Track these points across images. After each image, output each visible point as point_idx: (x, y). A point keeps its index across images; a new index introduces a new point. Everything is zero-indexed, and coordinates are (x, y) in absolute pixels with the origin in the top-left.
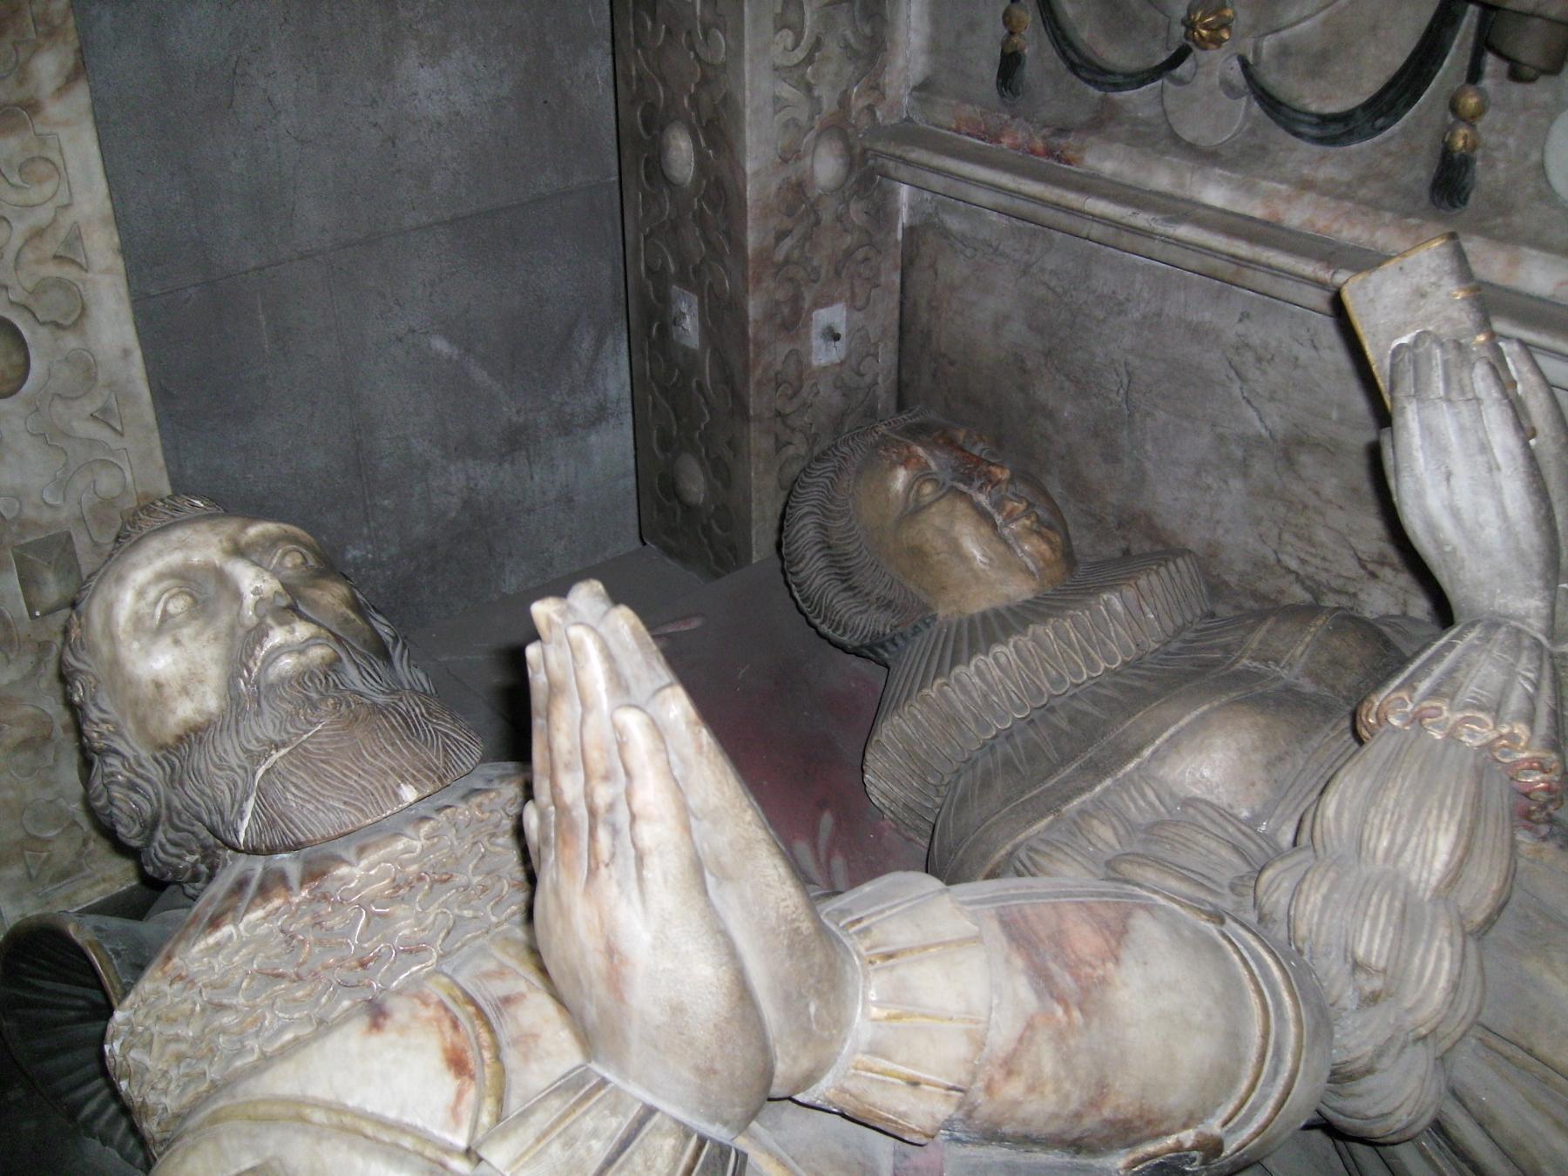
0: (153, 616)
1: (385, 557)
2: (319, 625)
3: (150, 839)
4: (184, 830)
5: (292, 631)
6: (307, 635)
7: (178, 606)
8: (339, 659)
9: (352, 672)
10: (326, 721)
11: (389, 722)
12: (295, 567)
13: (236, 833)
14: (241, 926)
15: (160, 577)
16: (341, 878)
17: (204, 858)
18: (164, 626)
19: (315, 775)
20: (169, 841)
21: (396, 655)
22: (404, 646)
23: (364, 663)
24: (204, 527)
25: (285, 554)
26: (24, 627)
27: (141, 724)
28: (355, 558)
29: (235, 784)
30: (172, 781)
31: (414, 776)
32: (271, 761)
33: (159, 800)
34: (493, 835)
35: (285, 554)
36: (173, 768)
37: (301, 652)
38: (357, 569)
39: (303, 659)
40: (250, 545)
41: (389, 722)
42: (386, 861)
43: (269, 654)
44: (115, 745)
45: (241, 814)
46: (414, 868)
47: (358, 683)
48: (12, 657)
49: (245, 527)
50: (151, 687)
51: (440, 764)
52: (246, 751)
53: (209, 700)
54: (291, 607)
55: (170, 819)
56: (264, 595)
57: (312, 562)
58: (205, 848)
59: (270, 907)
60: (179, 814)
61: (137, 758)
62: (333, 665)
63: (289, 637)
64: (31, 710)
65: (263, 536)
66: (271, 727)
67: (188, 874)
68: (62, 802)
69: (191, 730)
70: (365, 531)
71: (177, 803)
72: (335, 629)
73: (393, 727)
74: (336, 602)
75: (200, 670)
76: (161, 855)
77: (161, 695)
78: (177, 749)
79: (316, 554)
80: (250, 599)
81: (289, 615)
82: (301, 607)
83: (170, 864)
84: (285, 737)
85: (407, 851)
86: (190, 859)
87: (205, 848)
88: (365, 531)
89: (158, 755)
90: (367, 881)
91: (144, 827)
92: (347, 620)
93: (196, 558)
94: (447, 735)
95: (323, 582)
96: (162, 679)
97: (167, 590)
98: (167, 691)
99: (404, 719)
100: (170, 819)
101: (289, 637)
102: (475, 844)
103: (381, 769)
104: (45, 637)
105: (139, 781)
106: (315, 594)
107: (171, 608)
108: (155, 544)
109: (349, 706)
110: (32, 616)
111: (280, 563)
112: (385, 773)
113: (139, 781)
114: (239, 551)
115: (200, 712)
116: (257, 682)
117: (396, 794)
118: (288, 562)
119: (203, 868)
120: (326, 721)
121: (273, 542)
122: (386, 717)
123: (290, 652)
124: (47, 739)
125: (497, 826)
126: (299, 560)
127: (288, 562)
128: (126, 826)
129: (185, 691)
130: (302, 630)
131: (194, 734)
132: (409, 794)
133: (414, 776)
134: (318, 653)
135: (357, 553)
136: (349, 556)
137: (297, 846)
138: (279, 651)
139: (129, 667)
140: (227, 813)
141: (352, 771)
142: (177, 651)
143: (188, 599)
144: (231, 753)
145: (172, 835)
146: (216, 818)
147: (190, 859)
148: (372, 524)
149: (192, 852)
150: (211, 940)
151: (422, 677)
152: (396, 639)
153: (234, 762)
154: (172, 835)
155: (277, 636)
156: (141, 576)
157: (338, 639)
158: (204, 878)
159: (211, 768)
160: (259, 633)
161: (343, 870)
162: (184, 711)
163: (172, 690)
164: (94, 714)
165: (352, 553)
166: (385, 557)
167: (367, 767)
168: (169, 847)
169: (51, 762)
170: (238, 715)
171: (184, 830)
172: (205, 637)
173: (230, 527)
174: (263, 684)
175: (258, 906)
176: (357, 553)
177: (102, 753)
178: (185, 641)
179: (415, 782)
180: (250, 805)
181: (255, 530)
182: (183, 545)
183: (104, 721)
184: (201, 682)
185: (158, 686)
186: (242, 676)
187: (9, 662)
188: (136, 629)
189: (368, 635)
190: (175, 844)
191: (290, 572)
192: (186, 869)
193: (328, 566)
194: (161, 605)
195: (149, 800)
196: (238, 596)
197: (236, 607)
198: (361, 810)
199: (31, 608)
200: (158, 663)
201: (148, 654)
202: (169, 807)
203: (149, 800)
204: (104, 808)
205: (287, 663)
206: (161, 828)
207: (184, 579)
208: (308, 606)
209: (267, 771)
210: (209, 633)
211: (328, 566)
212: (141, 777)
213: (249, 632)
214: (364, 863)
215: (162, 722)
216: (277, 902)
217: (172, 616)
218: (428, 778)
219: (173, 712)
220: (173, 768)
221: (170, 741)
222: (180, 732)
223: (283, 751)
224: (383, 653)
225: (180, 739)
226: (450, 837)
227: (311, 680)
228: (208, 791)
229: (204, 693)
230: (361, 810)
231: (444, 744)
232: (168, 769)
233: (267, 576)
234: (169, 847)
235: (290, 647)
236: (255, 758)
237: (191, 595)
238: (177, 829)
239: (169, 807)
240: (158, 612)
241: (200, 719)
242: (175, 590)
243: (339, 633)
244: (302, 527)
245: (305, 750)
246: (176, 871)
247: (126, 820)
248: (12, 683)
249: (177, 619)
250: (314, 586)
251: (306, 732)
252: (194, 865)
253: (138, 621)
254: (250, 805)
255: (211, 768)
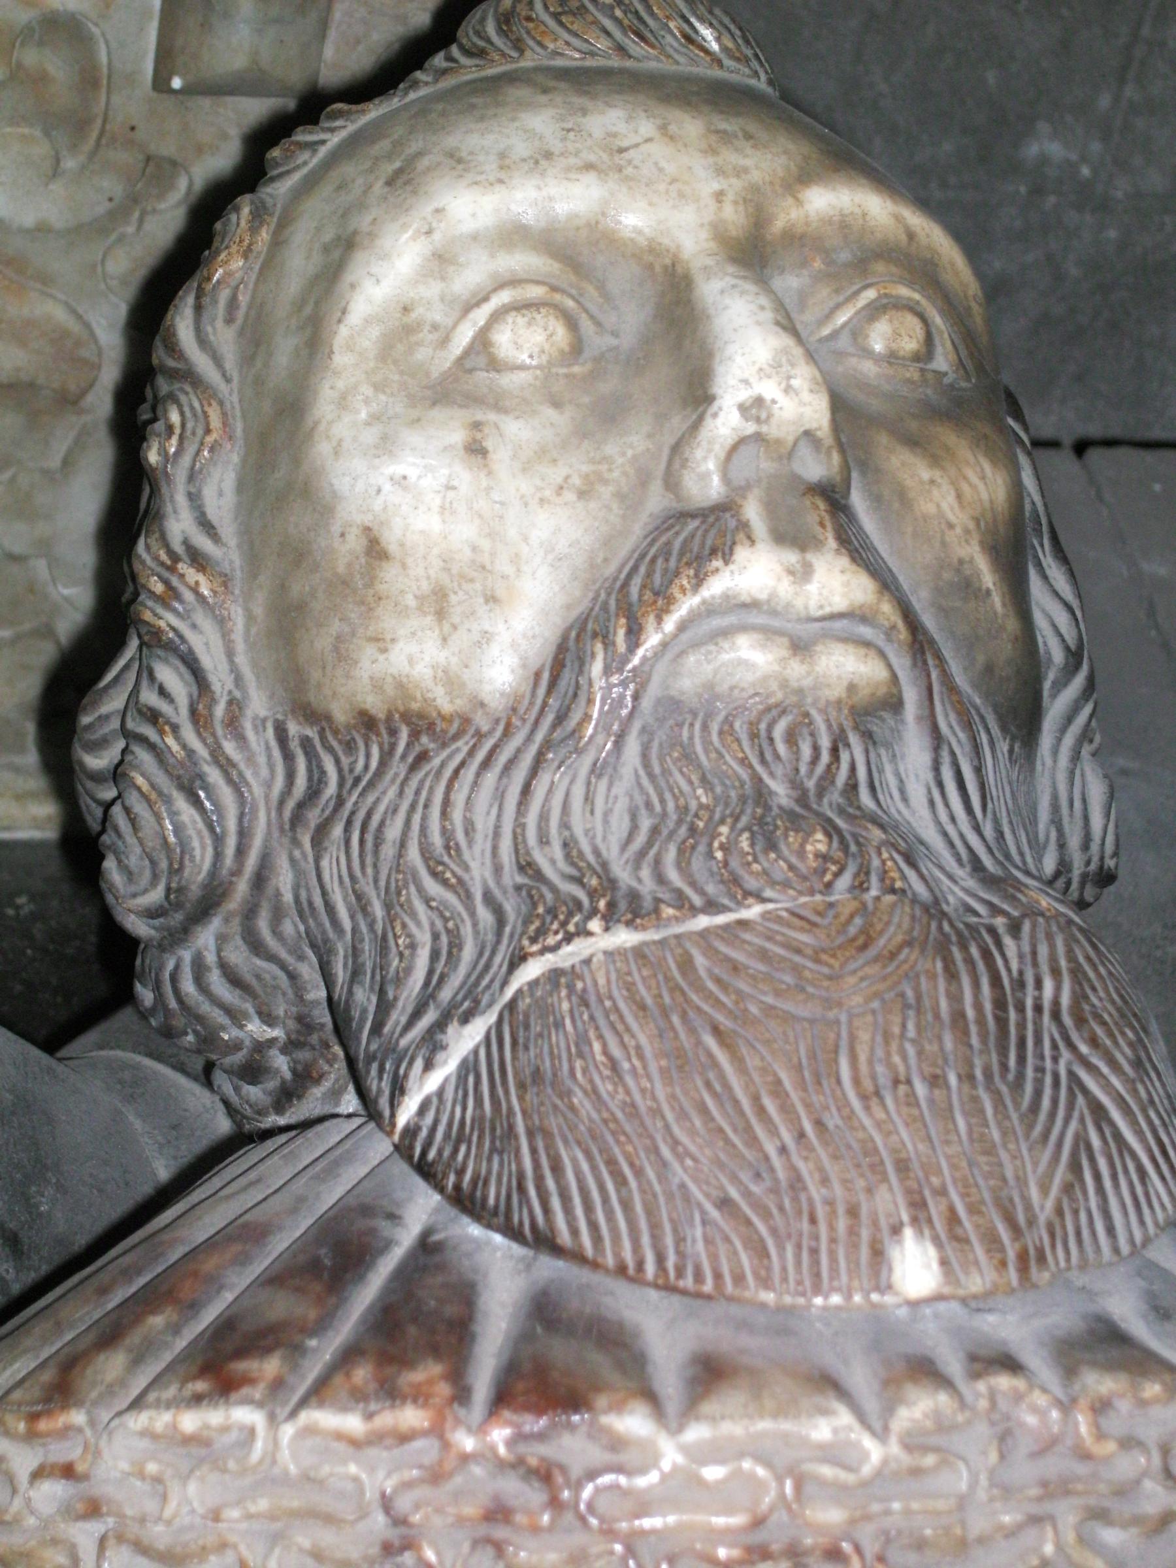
0: (445, 341)
1: (1121, 188)
2: (886, 582)
3: (179, 936)
4: (272, 958)
5: (804, 573)
6: (839, 603)
7: (526, 342)
8: (894, 704)
9: (915, 754)
10: (781, 902)
11: (956, 998)
12: (892, 357)
13: (399, 1089)
14: (288, 1431)
15: (512, 235)
16: (617, 1443)
17: (291, 1046)
18: (461, 389)
19: (680, 1063)
20: (224, 966)
21: (1055, 708)
22: (1090, 687)
23: (956, 737)
24: (691, 126)
25: (875, 311)
26: (131, 103)
27: (287, 623)
28: (1044, 160)
29: (456, 945)
30: (297, 819)
31: (953, 1218)
32: (570, 954)
33: (241, 852)
34: (1100, 1515)
35: (875, 311)
36: (314, 792)
37: (800, 647)
38: (1038, 191)
39: (796, 670)
40: (800, 241)
41: (956, 998)
42: (759, 1459)
43: (709, 610)
44: (195, 641)
45: (432, 1045)
46: (831, 1516)
47: (917, 793)
48: (70, 164)
49: (804, 177)
50: (356, 542)
51: (1045, 1209)
52: (526, 866)
53: (499, 661)
54: (826, 510)
55: (250, 913)
56: (772, 431)
57: (942, 361)
58: (305, 1024)
59: (387, 1419)
60: (278, 915)
61: (236, 706)
62: (871, 715)
63: (785, 589)
64: (60, 314)
65: (843, 224)
66: (620, 825)
67: (238, 1058)
68: (40, 566)
69: (406, 717)
70: (1104, 101)
71: (284, 880)
72: (921, 602)
73: (959, 1016)
74: (959, 518)
75: (503, 566)
76: (188, 986)
77: (371, 579)
78: (350, 747)
79: (966, 336)
80: (725, 422)
81: (815, 513)
82: (858, 500)
83: (200, 1019)
84: (647, 886)
85: (829, 1453)
86: (255, 1028)
87: (305, 1024)
88: (1104, 101)
89: (293, 728)
90: (685, 1487)
91: (175, 897)
92: (968, 587)
93: (634, 219)
94: (1098, 1110)
95: (949, 436)
96: (391, 539)
97: (513, 282)
98: (390, 577)
99: (1000, 1004)
100: (250, 913)
101: (785, 589)
102: (1035, 1520)
103: (870, 1149)
104: (167, 149)
105: (214, 775)
106: (910, 469)
107: (504, 340)
108: (541, 122)
109: (860, 886)
110: (160, 83)
111: (856, 331)
112: (877, 1167)
113: (214, 775)
114: (753, 252)
115: (450, 681)
116: (641, 679)
117: (878, 1254)
118: (879, 338)
119: (281, 1063)
120: (781, 902)
121: (862, 257)
122: (952, 975)
123: (768, 633)
124: (69, 401)
125: (1122, 1491)
126: (910, 345)
127: (879, 338)
128: (130, 875)
129: (438, 604)
130: (834, 584)
131: (413, 732)
132: (916, 1268)
133: (953, 1218)
134: (845, 668)
135: (1055, 150)
136: (1032, 150)
137: (543, 1241)
138: (745, 613)
139: (322, 448)
140: (398, 1016)
141: (786, 1108)
142: (465, 477)
143: (561, 333)
144: (482, 843)
145: (238, 955)
146: (364, 998)
147: (255, 1028)
148: (1130, 91)
149: (268, 1019)
150: (190, 1421)
151: (1097, 791)
152: (1075, 657)
153: (479, 873)
154: (238, 955)
155: (755, 571)
156: (466, 207)
157: (920, 643)
158: (272, 1084)
159: (413, 854)
160: (704, 536)
161: (634, 1423)
162: (409, 658)
163: (403, 582)
164: (179, 524)
165: (1046, 146)
166: (1121, 188)
167: (833, 1120)
168: (215, 979)
169: (55, 462)
170: (547, 745)
171: (272, 958)
172: (556, 474)
173: (765, 159)
174: (653, 691)
175: (358, 1396)
176: (1055, 150)
177: (154, 641)
178: (500, 455)
179: (951, 1239)
180: (466, 1039)
181: (832, 201)
182: (613, 162)
183: (198, 559)
184: (491, 599)
185: (375, 550)
186: (608, 644)
187: (56, 172)
188: (385, 352)
189: (1005, 650)
190: (234, 979)
191: (869, 368)
192: (237, 1046)
193: (989, 396)
194: (481, 315)
195: (219, 841)
196: (697, 393)
197: (678, 423)
198: (761, 1252)
199: (166, 59)
200: (402, 485)
201: (386, 446)
202: (260, 880)
203: (219, 841)
204: (97, 777)
205: (752, 660)
206: (216, 923)
207: (574, 261)
208: (877, 500)
209: (554, 976)
210: (574, 466)
211: (989, 396)
212: (225, 766)
213: (684, 515)
214: (696, 1433)
215: (342, 653)
216: (411, 1416)
217: (495, 365)
218: (992, 1241)
219: (382, 643)
220: (314, 792)
221: (341, 715)
222: (374, 704)
223: (624, 937)
224: (1023, 719)
225: (367, 722)
226: (977, 1446)
227: (791, 738)
228: (378, 911)
229: (487, 637)
230: (761, 1252)
231: (1081, 1140)
232: (301, 782)
233: (803, 376)
234: (215, 979)
235: (784, 621)
236: (547, 912)
237: (572, 324)
238: (256, 946)
239: (260, 880)
240: (465, 335)
241: (445, 703)
242: (535, 292)
243: (929, 620)
244: (957, 235)
245: (686, 965)
246: (208, 1040)
247: (134, 859)
248: (42, 229)
249: (510, 381)
250: (913, 442)
251: (712, 907)
252: (260, 1047)
253: (403, 329)
254: (466, 1039)
255: (413, 854)
